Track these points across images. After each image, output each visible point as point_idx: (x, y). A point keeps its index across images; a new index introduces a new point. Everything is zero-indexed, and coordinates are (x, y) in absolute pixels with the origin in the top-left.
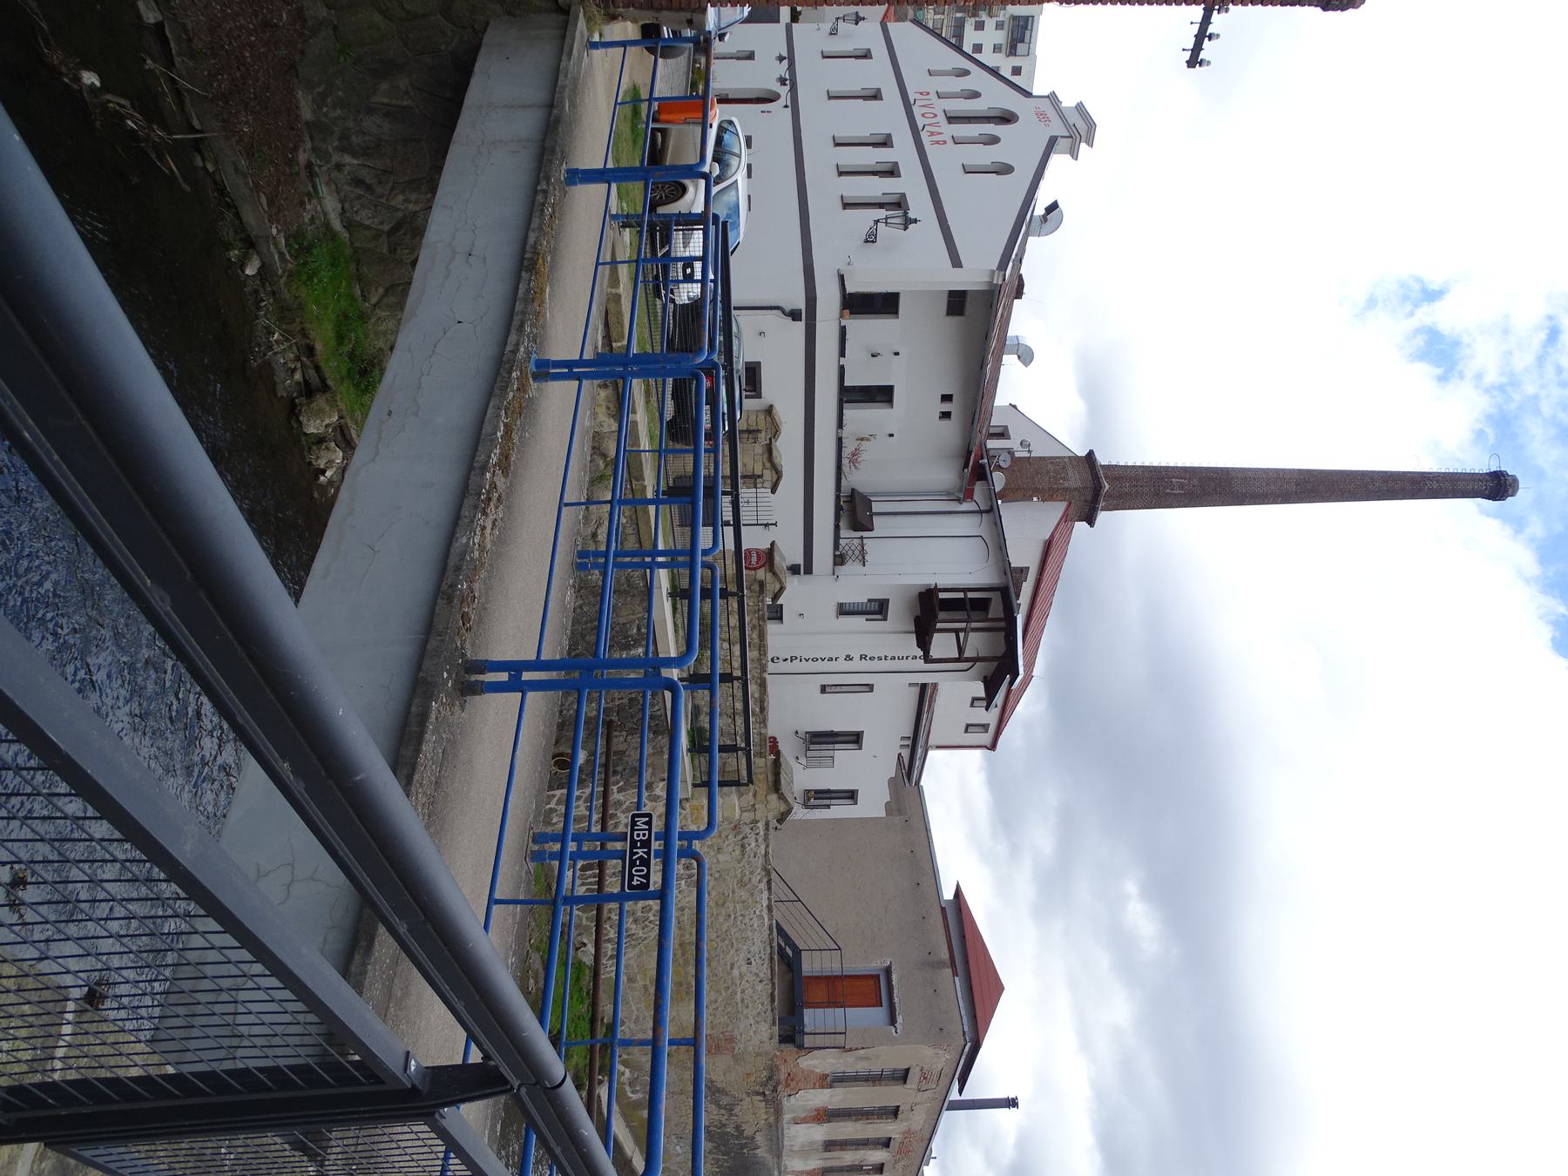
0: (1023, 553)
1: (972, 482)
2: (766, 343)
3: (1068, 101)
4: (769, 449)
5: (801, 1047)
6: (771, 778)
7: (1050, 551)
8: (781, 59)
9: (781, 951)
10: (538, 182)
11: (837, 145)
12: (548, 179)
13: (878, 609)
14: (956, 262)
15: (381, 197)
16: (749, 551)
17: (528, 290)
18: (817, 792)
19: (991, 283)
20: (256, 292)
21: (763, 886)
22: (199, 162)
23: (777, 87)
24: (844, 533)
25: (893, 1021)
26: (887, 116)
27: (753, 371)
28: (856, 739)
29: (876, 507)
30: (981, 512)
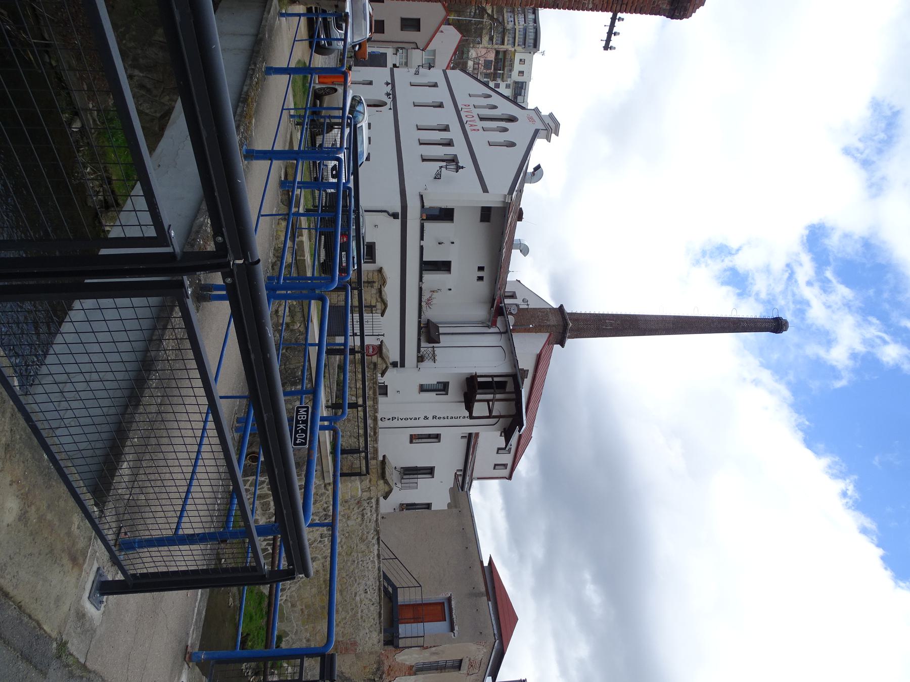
0: (526, 362)
1: (496, 316)
2: (380, 232)
3: (545, 112)
4: (380, 291)
5: (397, 647)
6: (380, 471)
7: (541, 360)
8: (387, 84)
9: (386, 590)
10: (250, 65)
11: (421, 144)
12: (255, 64)
13: (443, 388)
14: (485, 190)
15: (156, 96)
16: (368, 346)
17: (243, 111)
18: (408, 505)
19: (504, 202)
20: (77, 142)
21: (375, 541)
22: (47, 59)
23: (385, 99)
24: (423, 344)
25: (452, 629)
26: (447, 116)
27: (371, 248)
28: (430, 471)
29: (441, 330)
30: (500, 333)
